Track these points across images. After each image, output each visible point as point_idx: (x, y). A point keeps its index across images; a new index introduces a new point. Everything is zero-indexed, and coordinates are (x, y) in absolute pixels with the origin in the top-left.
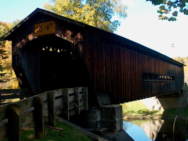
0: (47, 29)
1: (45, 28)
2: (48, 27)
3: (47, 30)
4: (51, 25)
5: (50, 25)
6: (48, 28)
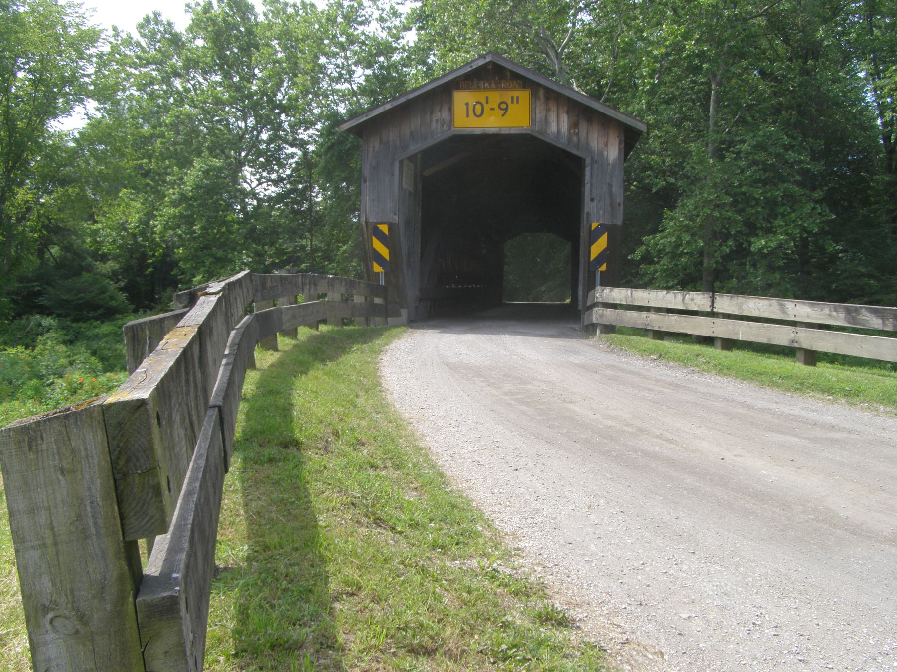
0: (503, 112)
1: (493, 109)
2: (503, 106)
3: (503, 115)
4: (517, 102)
5: (512, 102)
6: (506, 109)
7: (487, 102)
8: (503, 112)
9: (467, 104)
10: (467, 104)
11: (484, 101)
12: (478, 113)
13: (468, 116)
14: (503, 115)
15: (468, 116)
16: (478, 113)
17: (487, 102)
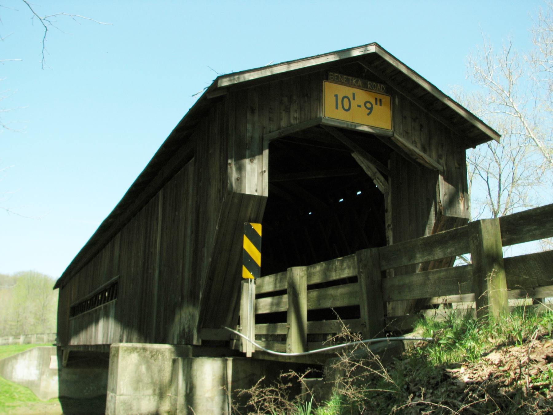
0: (368, 111)
1: (359, 106)
2: (369, 105)
3: (369, 114)
6: (371, 109)
7: (354, 99)
8: (368, 111)
9: (336, 96)
10: (336, 96)
11: (351, 98)
12: (346, 107)
13: (337, 108)
14: (369, 114)
15: (337, 108)
16: (346, 107)
17: (354, 99)
